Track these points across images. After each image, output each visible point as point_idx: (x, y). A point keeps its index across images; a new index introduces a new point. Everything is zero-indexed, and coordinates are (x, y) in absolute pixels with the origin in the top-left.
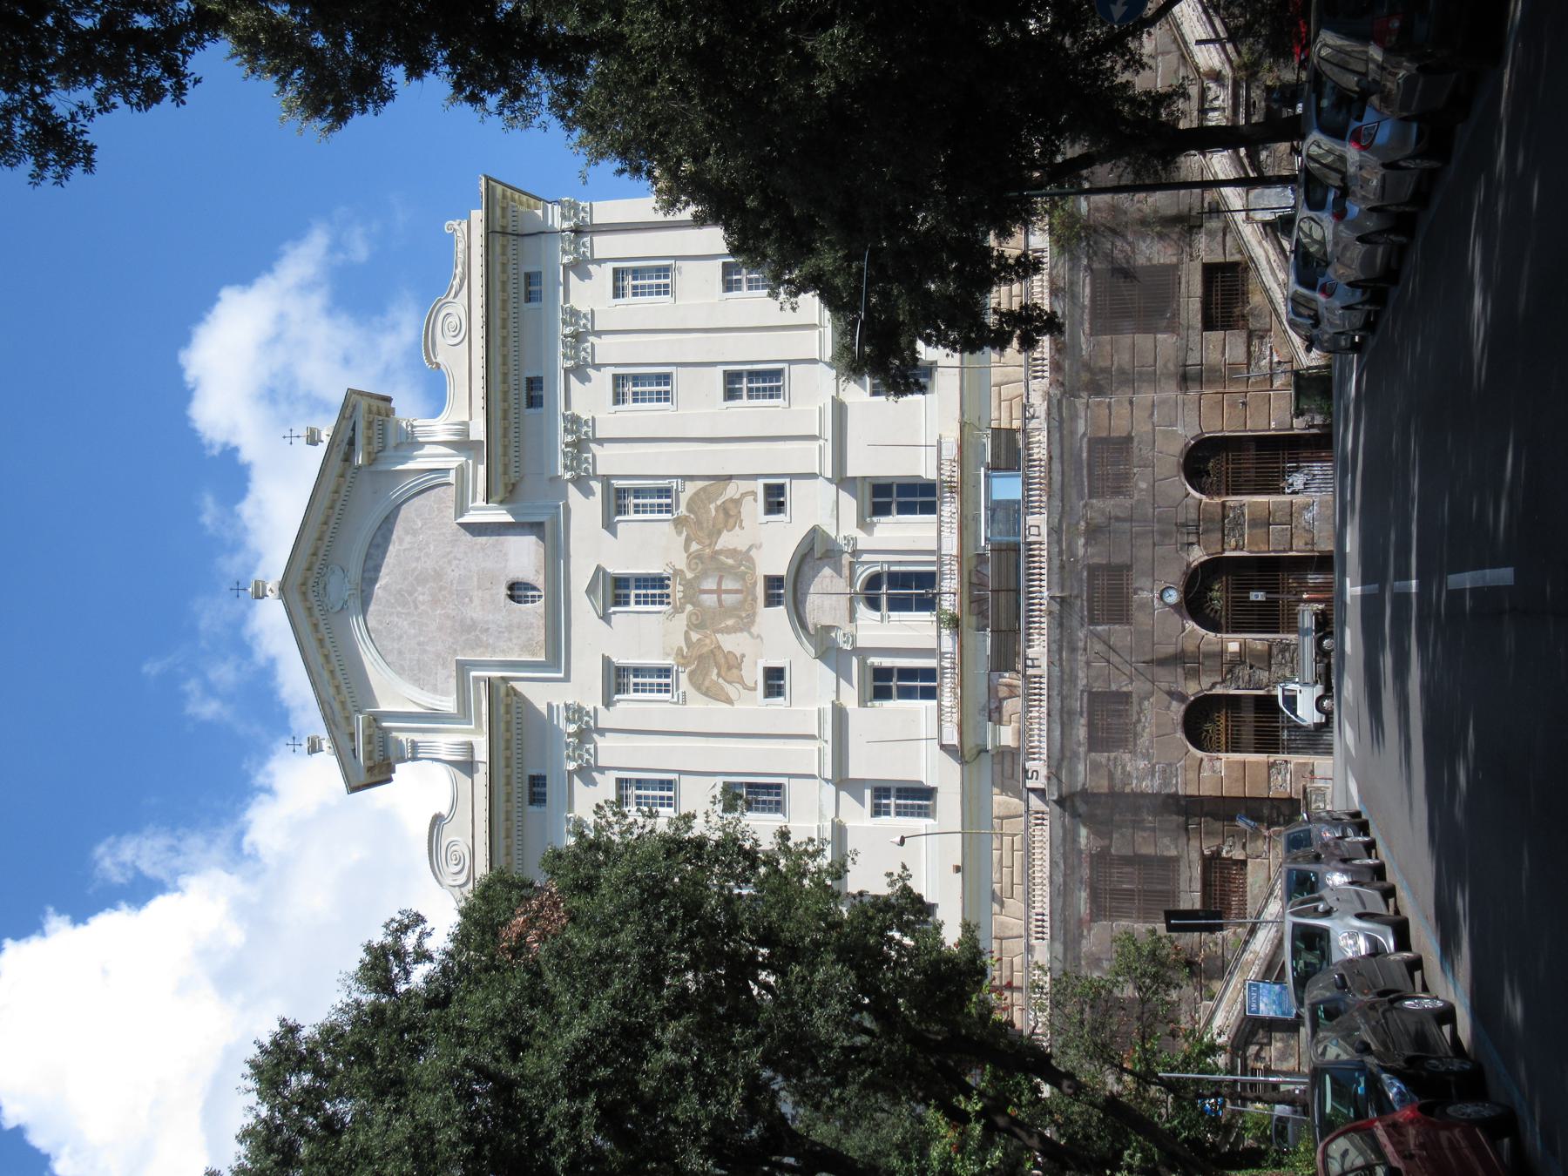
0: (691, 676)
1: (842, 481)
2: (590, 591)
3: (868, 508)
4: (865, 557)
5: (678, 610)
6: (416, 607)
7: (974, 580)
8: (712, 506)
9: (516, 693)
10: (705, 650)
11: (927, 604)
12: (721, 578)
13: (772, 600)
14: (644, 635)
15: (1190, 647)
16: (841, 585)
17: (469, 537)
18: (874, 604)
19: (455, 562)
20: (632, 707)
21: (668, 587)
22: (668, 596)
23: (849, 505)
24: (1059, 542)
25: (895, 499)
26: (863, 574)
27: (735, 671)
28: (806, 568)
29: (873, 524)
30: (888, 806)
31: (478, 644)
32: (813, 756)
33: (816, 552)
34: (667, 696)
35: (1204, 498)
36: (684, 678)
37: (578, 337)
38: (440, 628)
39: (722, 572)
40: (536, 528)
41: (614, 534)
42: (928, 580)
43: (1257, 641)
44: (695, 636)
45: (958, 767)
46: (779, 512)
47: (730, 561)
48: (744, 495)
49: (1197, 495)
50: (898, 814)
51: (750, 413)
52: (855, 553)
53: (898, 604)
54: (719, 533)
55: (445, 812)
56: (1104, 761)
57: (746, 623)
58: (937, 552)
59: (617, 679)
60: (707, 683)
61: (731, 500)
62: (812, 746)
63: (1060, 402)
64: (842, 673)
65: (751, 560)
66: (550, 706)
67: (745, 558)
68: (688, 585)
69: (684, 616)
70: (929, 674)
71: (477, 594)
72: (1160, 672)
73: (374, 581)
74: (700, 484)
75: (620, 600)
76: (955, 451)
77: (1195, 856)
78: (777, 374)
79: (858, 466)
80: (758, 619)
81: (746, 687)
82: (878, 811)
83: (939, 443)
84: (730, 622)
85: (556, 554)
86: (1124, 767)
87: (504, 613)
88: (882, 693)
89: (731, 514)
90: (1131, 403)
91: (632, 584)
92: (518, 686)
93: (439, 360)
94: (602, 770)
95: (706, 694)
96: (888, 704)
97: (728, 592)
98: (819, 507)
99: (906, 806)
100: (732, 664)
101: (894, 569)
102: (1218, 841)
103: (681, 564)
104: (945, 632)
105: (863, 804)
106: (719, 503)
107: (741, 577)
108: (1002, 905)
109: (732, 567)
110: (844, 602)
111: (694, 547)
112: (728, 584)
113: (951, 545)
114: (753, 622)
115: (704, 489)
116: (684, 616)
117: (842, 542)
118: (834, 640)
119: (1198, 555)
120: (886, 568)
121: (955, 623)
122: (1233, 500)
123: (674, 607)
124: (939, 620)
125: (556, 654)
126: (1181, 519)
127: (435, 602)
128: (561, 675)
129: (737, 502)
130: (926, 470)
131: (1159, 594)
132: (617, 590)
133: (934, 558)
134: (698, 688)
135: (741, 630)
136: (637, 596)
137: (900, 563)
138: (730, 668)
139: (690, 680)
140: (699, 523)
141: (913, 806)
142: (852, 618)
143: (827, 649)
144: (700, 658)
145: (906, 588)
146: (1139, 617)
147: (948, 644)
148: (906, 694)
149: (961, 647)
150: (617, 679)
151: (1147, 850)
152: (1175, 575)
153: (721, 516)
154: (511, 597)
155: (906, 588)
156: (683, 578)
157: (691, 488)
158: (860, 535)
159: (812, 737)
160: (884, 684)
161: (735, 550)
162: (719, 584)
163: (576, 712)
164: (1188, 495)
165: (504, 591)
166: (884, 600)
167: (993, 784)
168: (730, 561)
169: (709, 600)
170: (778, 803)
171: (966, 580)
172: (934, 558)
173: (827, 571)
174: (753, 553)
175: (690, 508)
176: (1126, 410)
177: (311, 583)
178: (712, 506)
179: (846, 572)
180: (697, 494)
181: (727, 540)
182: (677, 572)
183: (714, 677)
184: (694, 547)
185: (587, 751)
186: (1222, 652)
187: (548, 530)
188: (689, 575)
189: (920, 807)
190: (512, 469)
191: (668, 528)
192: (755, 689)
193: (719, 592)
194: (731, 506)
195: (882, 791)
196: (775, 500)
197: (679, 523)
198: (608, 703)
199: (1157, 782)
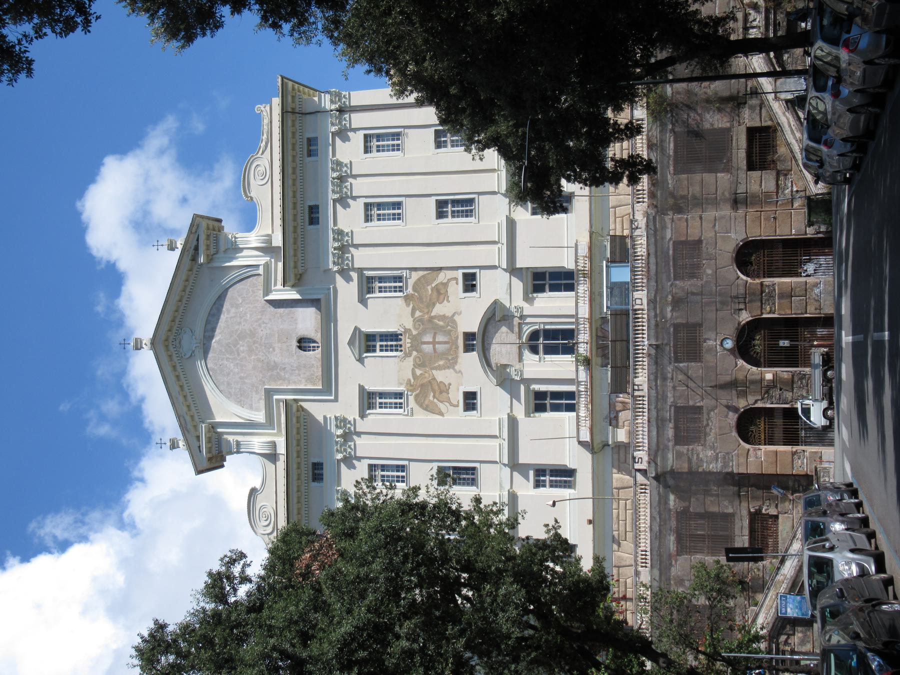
0: (416, 398)
1: (513, 270)
2: (351, 343)
3: (530, 288)
4: (529, 320)
5: (408, 355)
6: (239, 355)
7: (600, 334)
8: (429, 288)
9: (303, 409)
10: (426, 380)
11: (569, 350)
12: (435, 334)
13: (468, 348)
14: (386, 371)
15: (741, 376)
16: (513, 338)
17: (272, 309)
18: (534, 350)
19: (263, 325)
20: (377, 418)
21: (401, 340)
22: (401, 346)
23: (518, 286)
24: (655, 309)
25: (548, 282)
26: (527, 331)
27: (444, 394)
28: (490, 327)
29: (534, 298)
30: (544, 481)
31: (279, 378)
32: (496, 449)
33: (496, 317)
34: (401, 411)
35: (749, 279)
36: (411, 399)
37: (342, 179)
38: (254, 368)
39: (436, 330)
40: (315, 303)
41: (366, 306)
42: (569, 334)
43: (784, 372)
44: (418, 372)
45: (589, 456)
46: (473, 291)
47: (441, 323)
48: (449, 280)
49: (744, 278)
50: (551, 486)
51: (454, 227)
52: (522, 317)
53: (551, 350)
54: (434, 305)
55: (258, 486)
56: (685, 451)
57: (452, 364)
58: (576, 316)
59: (369, 400)
60: (426, 402)
61: (442, 283)
62: (495, 443)
63: (654, 218)
64: (514, 395)
65: (454, 322)
66: (325, 418)
67: (450, 321)
68: (414, 338)
69: (411, 359)
70: (571, 395)
71: (277, 346)
72: (720, 393)
73: (212, 337)
74: (421, 273)
75: (370, 349)
76: (587, 250)
77: (745, 513)
78: (470, 202)
79: (522, 262)
80: (459, 360)
81: (452, 405)
82: (538, 484)
83: (576, 245)
84: (441, 363)
85: (329, 319)
86: (698, 455)
87: (295, 357)
88: (540, 408)
89: (441, 293)
90: (701, 218)
91: (378, 338)
92: (305, 405)
93: (252, 195)
94: (359, 459)
95: (426, 409)
96: (544, 415)
97: (439, 343)
98: (498, 287)
99: (556, 481)
100: (443, 390)
101: (547, 327)
102: (760, 503)
103: (409, 325)
104: (581, 368)
105: (528, 480)
106: (433, 285)
107: (448, 333)
108: (619, 545)
109: (442, 327)
110: (515, 349)
111: (418, 314)
112: (440, 338)
113: (584, 311)
114: (456, 363)
115: (423, 276)
116: (411, 359)
117: (513, 310)
118: (509, 374)
119: (745, 317)
120: (542, 327)
121: (587, 362)
122: (768, 281)
123: (405, 353)
124: (577, 361)
125: (329, 384)
126: (734, 294)
127: (251, 351)
128: (333, 398)
129: (445, 285)
130: (568, 264)
131: (720, 342)
132: (368, 342)
133: (574, 320)
134: (421, 406)
135: (449, 368)
136: (381, 346)
137: (551, 323)
138: (441, 392)
139: (416, 400)
140: (421, 299)
141: (560, 481)
142: (520, 359)
143: (505, 379)
144: (422, 386)
145: (556, 340)
146: (707, 357)
147: (583, 375)
148: (556, 408)
149: (591, 377)
150: (369, 400)
151: (714, 509)
152: (730, 330)
153: (435, 293)
154: (300, 347)
155: (556, 340)
156: (411, 334)
157: (415, 276)
158: (525, 305)
159: (495, 437)
160: (541, 402)
161: (444, 316)
162: (434, 338)
163: (342, 422)
164: (738, 278)
165: (295, 344)
166: (541, 347)
167: (613, 466)
168: (441, 323)
169: (428, 348)
170: (473, 479)
171: (594, 335)
172: (574, 320)
173: (504, 329)
174: (456, 318)
175: (414, 289)
176: (697, 223)
177: (171, 339)
178: (429, 288)
179: (516, 329)
180: (419, 280)
181: (439, 309)
182: (407, 331)
183: (431, 398)
184: (418, 314)
185: (350, 447)
186: (762, 380)
187: (322, 303)
188: (415, 332)
189: (565, 482)
190: (299, 265)
191: (401, 302)
192: (458, 406)
193: (434, 343)
194: (441, 287)
195: (540, 472)
196: (470, 283)
197: (407, 298)
198: (362, 415)
199: (720, 465)
